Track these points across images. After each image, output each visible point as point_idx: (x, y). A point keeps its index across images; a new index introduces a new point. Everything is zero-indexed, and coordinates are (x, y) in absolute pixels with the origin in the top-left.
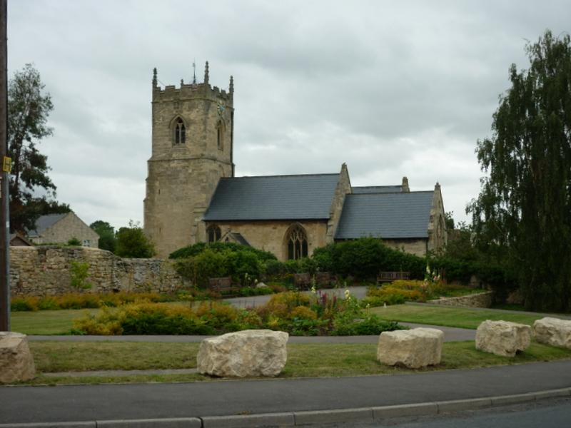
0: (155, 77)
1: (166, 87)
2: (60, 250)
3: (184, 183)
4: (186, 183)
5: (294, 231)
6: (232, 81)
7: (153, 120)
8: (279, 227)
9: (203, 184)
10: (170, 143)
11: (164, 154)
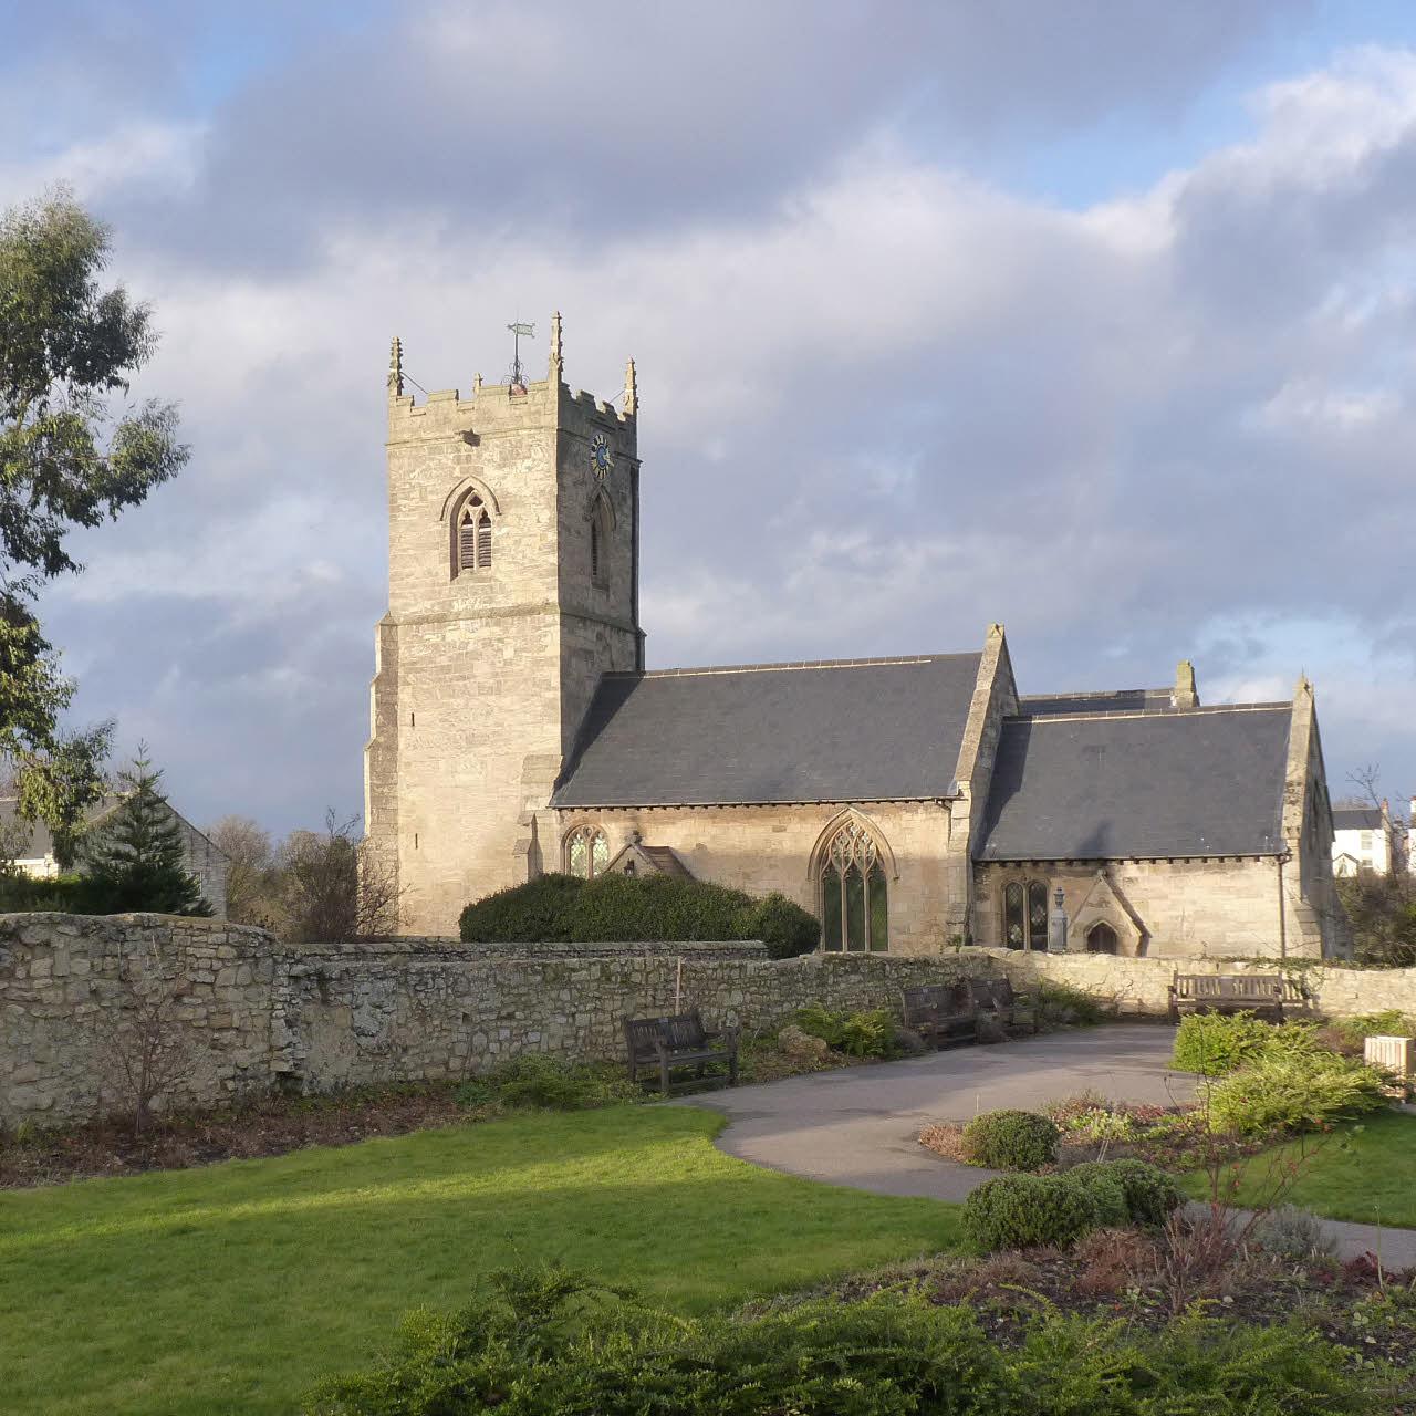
3: (491, 691)
4: (497, 690)
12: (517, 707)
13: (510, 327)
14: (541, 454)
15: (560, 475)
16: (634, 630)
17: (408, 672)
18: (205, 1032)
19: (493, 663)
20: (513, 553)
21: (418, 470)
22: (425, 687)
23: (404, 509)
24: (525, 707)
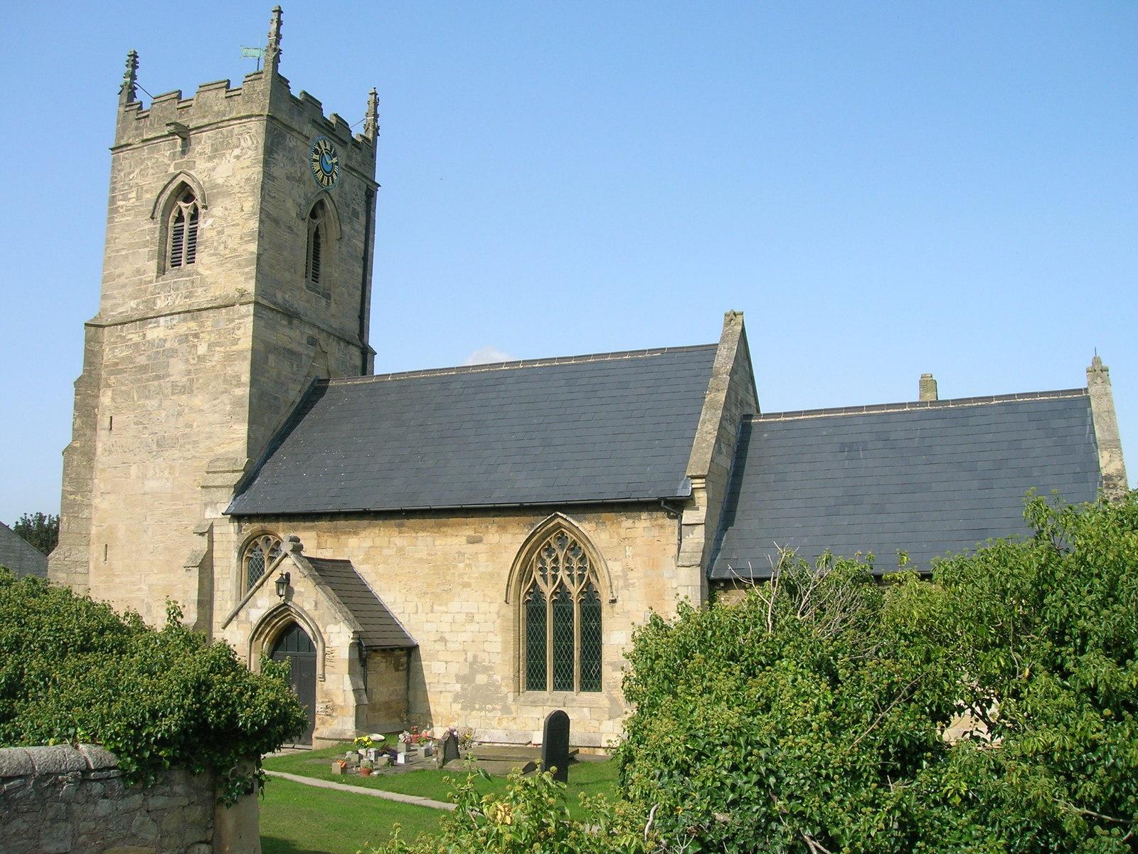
4: (187, 390)
12: (205, 407)
14: (250, 142)
15: (266, 163)
17: (111, 373)
19: (187, 360)
21: (137, 171)
22: (124, 388)
23: (121, 211)
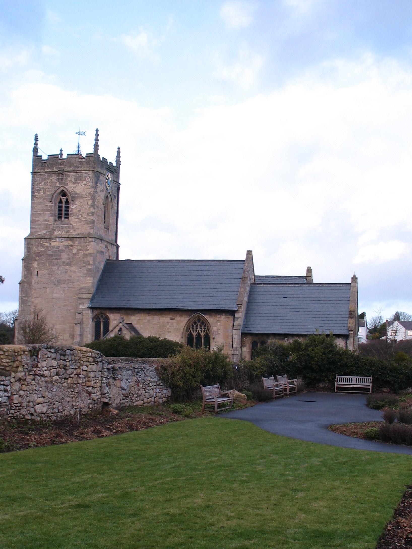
0: (36, 144)
1: (49, 156)
2: (53, 350)
3: (67, 264)
4: (69, 264)
5: (195, 323)
6: (119, 152)
7: (33, 192)
8: (178, 318)
9: (89, 267)
10: (51, 220)
11: (44, 232)
13: (77, 133)
16: (116, 245)
18: (85, 387)
20: (77, 215)
22: (42, 262)
24: (80, 271)
